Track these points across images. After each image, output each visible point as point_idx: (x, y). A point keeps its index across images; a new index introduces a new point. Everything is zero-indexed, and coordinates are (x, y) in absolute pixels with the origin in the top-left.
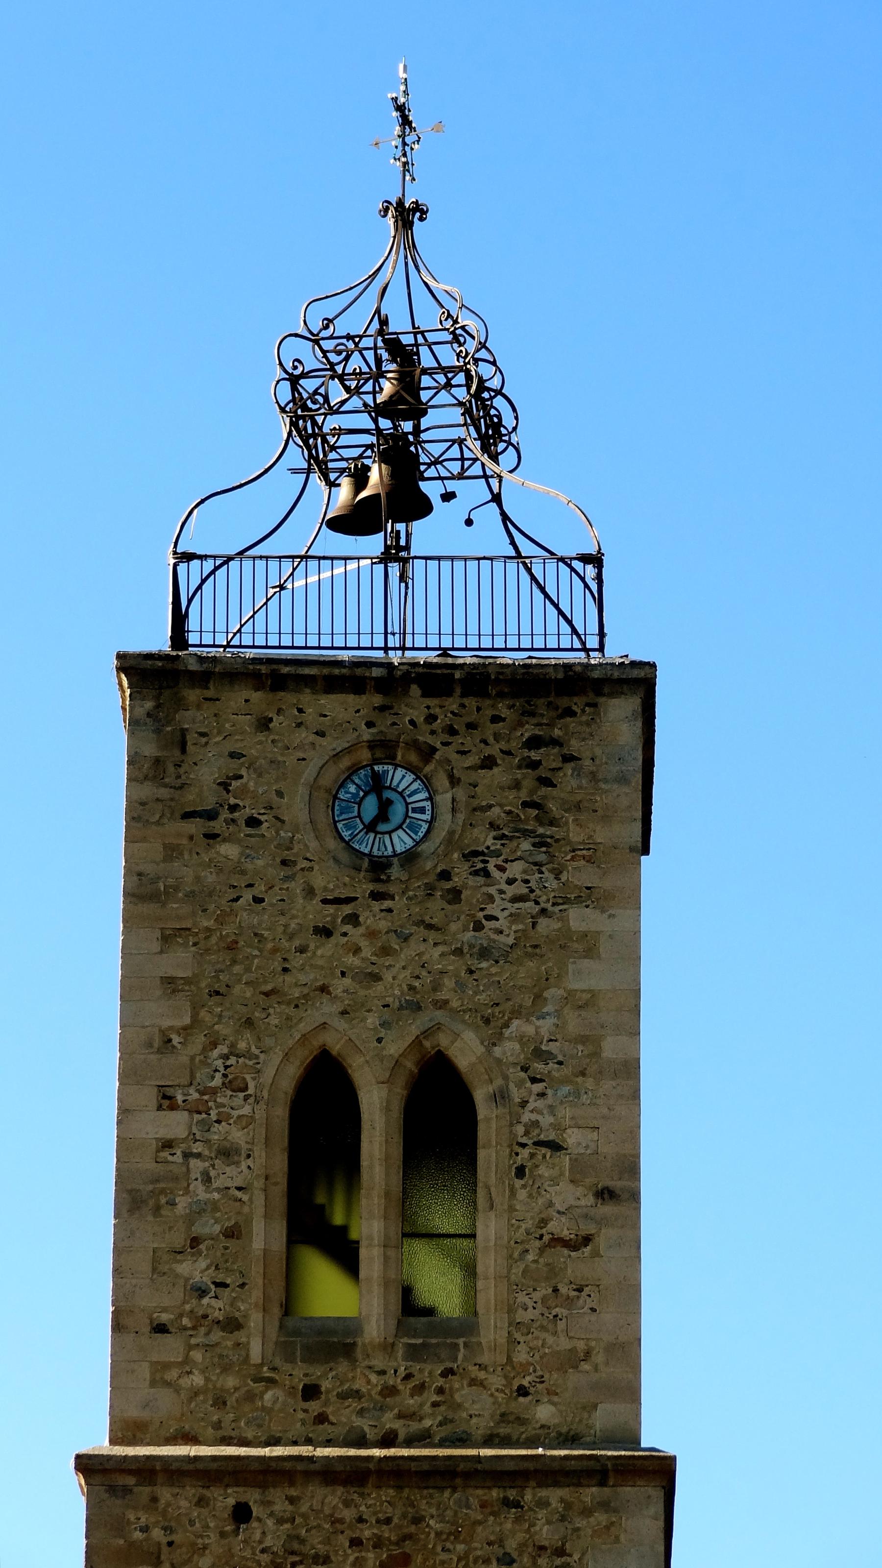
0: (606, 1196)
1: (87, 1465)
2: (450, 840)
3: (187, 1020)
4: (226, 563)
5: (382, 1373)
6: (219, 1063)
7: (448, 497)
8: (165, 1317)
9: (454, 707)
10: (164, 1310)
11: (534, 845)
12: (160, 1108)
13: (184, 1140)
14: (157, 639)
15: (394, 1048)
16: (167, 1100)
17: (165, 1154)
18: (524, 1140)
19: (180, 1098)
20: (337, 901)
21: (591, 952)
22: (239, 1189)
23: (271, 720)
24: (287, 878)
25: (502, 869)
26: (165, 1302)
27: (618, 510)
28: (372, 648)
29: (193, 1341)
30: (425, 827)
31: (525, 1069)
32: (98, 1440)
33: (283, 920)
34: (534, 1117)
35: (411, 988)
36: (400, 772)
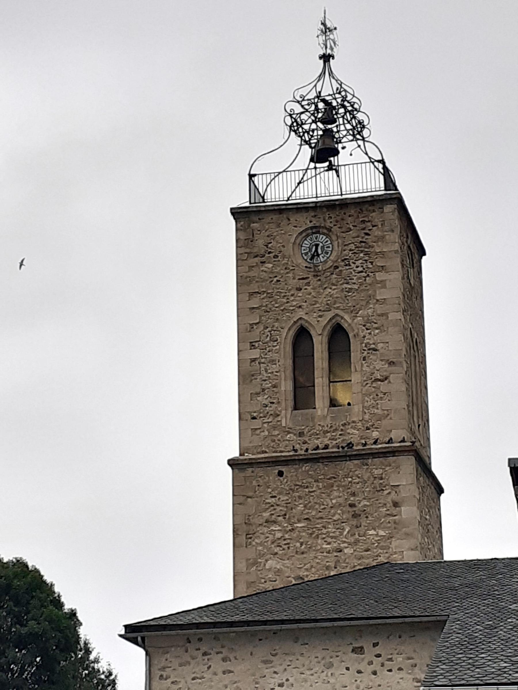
0: (392, 363)
1: (232, 463)
2: (338, 257)
3: (258, 321)
4: (278, 175)
5: (323, 426)
6: (269, 333)
7: (343, 148)
8: (255, 414)
9: (337, 213)
10: (255, 412)
11: (364, 254)
12: (251, 349)
13: (259, 358)
14: (243, 200)
15: (324, 321)
16: (252, 346)
17: (253, 363)
18: (365, 348)
19: (257, 345)
20: (303, 279)
21: (384, 287)
22: (277, 372)
23: (280, 224)
24: (287, 273)
25: (354, 263)
26: (254, 408)
27: (404, 149)
28: (312, 198)
29: (264, 421)
30: (330, 252)
31: (364, 326)
32: (235, 453)
33: (286, 286)
34: (368, 341)
35: (328, 304)
36: (321, 236)
